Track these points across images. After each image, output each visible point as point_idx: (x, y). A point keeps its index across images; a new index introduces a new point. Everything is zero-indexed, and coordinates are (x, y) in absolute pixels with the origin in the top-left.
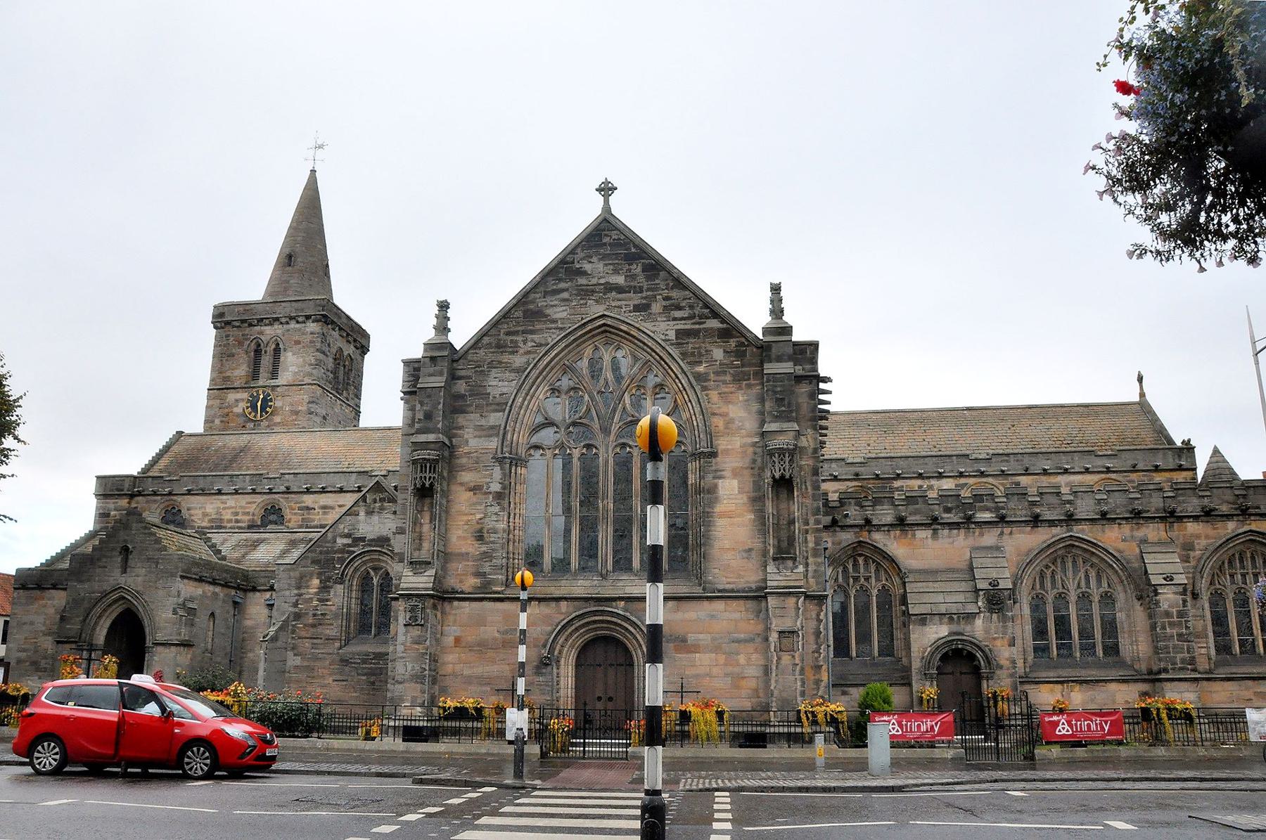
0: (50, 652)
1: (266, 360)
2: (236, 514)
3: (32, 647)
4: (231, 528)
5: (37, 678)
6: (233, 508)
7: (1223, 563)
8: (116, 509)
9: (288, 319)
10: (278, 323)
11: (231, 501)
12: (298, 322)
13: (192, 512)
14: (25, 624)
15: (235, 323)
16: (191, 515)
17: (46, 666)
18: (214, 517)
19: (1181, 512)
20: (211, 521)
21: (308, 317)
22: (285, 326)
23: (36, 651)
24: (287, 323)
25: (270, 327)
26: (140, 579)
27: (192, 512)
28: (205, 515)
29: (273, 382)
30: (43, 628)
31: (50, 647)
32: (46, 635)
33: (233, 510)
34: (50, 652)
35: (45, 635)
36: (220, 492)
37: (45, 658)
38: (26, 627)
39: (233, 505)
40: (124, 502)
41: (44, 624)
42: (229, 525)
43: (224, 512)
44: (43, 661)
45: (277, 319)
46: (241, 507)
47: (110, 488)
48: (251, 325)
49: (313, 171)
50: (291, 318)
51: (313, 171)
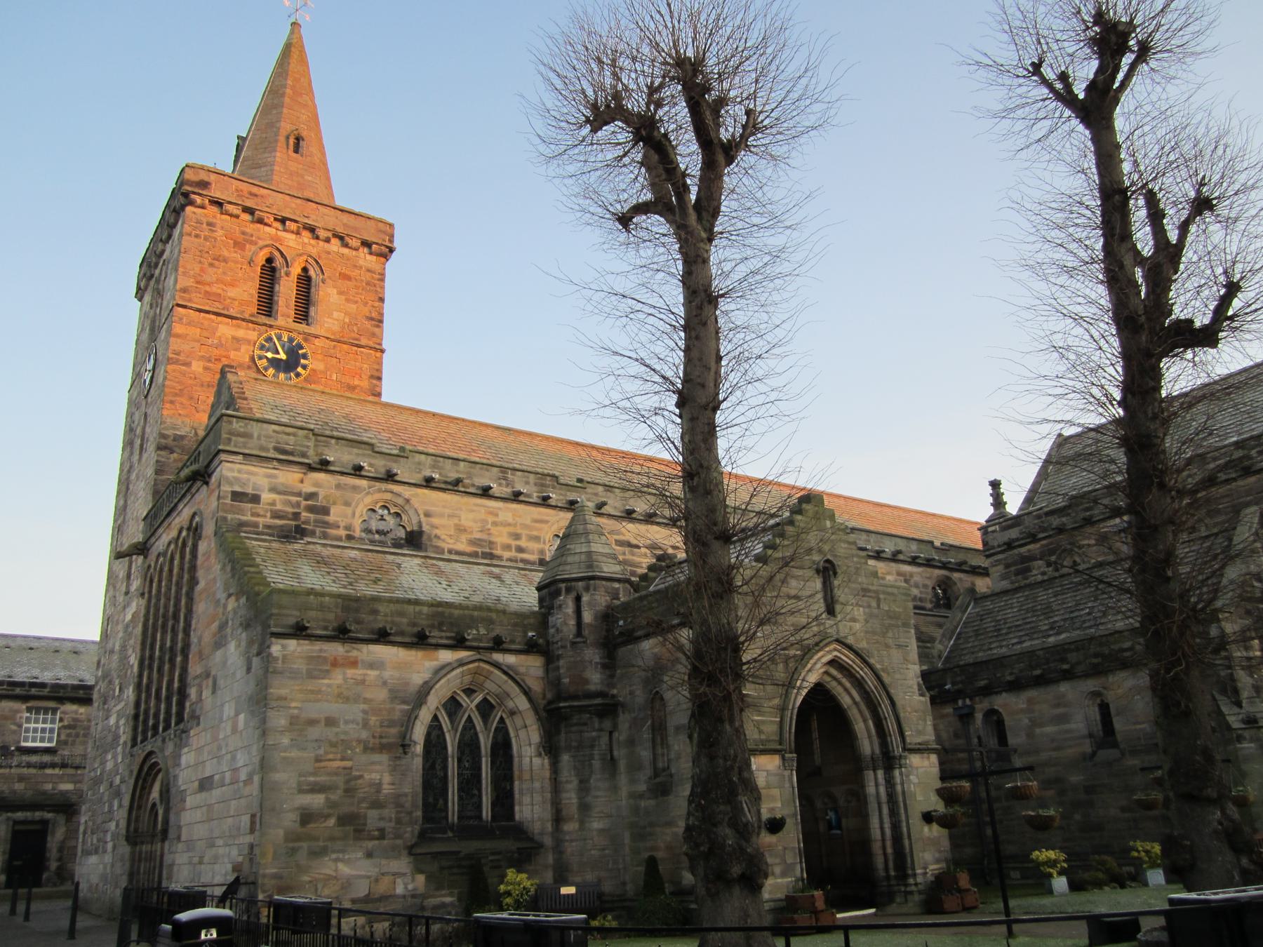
0: (387, 789)
1: (287, 290)
2: (517, 537)
3: (340, 781)
4: (510, 560)
5: (360, 855)
6: (509, 525)
7: (142, 742)
8: (273, 490)
9: (330, 235)
10: (366, 250)
11: (508, 512)
12: (346, 245)
13: (435, 521)
14: (312, 722)
15: (230, 208)
16: (434, 527)
17: (382, 824)
18: (478, 536)
19: (474, 640)
20: (472, 542)
21: (366, 244)
22: (321, 243)
23: (349, 791)
24: (327, 240)
25: (294, 236)
26: (857, 626)
27: (435, 521)
28: (461, 530)
29: (302, 327)
30: (364, 735)
31: (387, 778)
32: (373, 750)
33: (511, 529)
34: (387, 789)
35: (367, 749)
36: (485, 492)
37: (376, 805)
38: (314, 732)
39: (510, 520)
40: (290, 477)
41: (365, 725)
42: (506, 555)
43: (494, 530)
44: (373, 814)
45: (312, 230)
46: (525, 526)
47: (1005, 503)
48: (260, 221)
49: (291, 54)
50: (336, 236)
51: (291, 54)
